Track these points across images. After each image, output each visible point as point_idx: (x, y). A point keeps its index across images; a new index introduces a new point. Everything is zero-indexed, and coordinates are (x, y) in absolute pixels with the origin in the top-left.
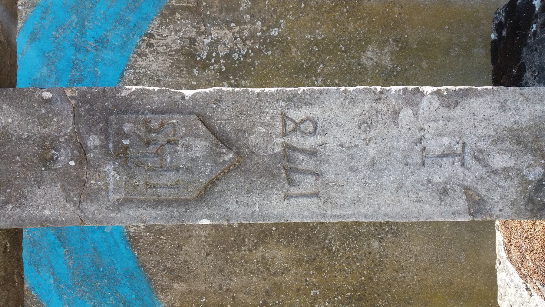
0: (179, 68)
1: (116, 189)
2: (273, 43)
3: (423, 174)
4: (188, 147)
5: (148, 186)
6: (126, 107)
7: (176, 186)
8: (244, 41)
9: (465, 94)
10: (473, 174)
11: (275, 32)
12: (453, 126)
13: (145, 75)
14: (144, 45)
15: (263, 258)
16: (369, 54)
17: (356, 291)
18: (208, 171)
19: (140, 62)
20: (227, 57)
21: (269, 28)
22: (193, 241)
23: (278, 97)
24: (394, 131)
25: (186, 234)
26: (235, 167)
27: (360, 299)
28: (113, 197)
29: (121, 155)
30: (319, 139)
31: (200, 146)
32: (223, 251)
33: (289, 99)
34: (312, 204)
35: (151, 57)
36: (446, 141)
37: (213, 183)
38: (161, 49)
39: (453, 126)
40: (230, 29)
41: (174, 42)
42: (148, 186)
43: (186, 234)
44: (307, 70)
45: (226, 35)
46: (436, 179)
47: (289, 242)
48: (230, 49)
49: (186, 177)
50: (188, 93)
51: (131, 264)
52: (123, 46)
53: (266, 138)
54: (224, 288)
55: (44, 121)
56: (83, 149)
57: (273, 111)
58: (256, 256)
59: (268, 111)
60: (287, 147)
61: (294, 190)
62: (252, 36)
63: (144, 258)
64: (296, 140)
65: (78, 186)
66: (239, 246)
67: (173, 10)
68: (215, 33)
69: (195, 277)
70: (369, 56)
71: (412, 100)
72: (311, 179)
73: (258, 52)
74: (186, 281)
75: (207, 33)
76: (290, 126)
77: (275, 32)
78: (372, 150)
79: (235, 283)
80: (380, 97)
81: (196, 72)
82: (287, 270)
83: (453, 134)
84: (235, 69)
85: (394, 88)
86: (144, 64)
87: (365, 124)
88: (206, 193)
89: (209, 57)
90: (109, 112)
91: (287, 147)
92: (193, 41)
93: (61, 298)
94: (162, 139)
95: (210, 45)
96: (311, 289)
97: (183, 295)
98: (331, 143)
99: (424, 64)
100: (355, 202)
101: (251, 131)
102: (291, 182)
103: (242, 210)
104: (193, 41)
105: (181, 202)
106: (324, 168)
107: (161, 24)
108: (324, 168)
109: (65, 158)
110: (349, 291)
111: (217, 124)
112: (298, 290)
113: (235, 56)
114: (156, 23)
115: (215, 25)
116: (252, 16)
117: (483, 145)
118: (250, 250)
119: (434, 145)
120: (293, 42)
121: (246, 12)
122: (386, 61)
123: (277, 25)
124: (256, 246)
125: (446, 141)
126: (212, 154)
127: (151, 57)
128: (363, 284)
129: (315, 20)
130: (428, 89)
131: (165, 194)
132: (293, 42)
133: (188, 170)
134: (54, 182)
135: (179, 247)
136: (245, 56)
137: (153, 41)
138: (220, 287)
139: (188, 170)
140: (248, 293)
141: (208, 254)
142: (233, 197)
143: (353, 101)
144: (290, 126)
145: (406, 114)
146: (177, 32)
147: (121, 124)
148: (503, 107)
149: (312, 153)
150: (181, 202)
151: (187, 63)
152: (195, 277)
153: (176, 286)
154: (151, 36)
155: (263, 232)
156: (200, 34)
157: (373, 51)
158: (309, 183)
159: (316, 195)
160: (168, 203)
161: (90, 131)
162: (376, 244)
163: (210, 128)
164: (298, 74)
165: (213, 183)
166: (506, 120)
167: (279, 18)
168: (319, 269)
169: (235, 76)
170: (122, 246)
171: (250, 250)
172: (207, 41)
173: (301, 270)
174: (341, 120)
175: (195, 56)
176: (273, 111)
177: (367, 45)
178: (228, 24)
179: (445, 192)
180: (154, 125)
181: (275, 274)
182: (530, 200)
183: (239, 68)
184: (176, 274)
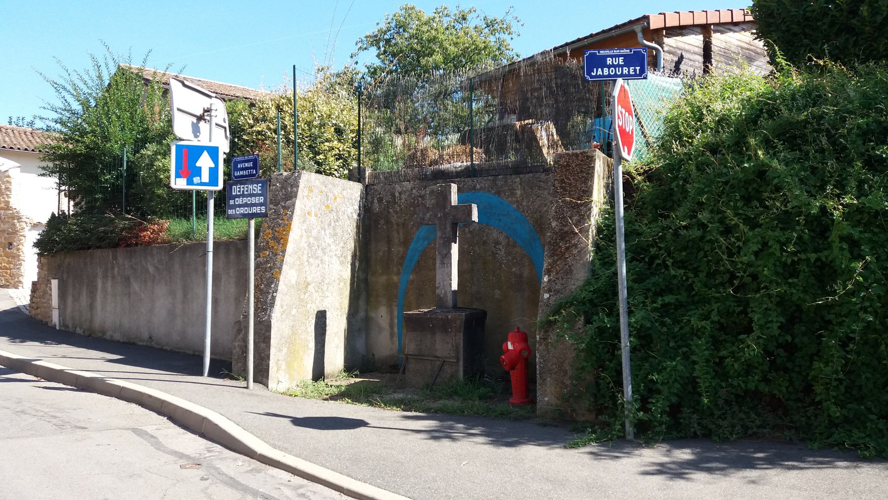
2: (500, 265)
65: (441, 237)
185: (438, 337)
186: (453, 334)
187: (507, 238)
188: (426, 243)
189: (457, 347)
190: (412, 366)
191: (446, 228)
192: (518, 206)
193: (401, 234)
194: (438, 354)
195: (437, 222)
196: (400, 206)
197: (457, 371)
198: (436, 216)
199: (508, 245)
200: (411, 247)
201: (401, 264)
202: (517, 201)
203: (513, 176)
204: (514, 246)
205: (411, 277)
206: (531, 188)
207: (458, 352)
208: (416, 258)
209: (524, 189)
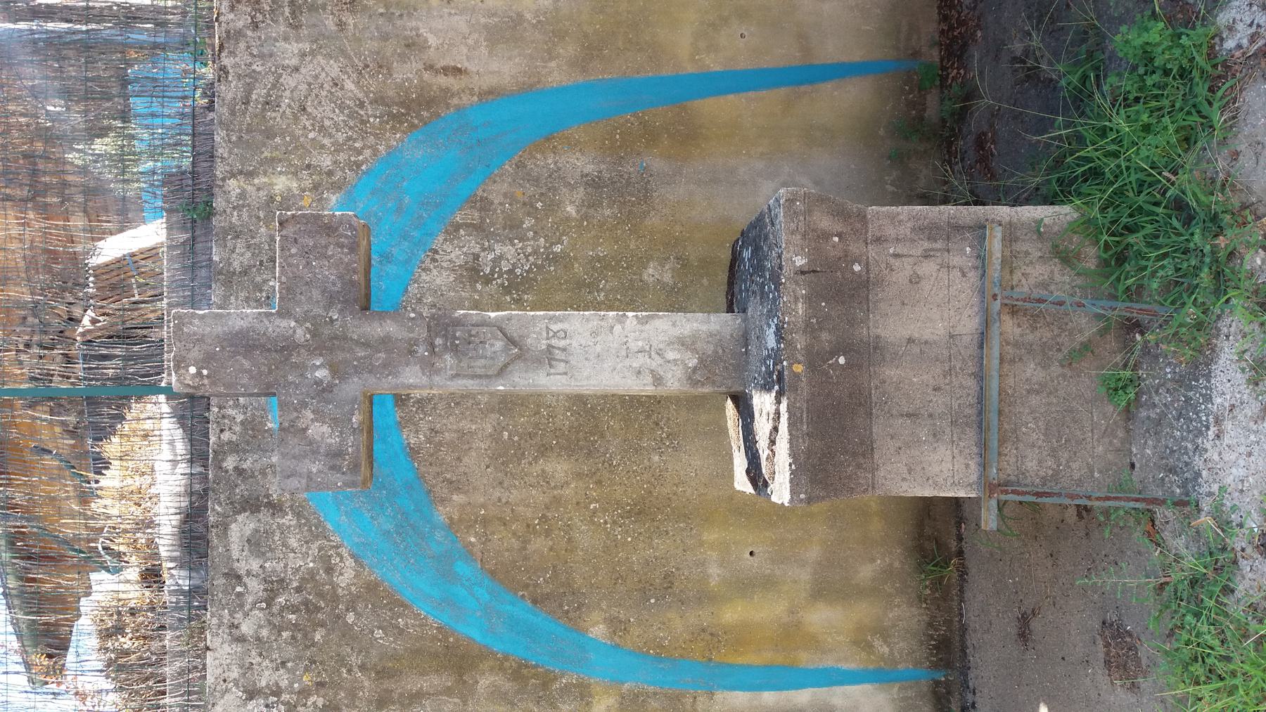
0: (462, 282)
1: (451, 368)
2: (555, 259)
3: (627, 362)
4: (492, 345)
5: (469, 367)
6: (458, 323)
7: (485, 367)
8: (527, 257)
9: (652, 317)
10: (656, 363)
11: (558, 248)
12: (644, 335)
13: (429, 289)
14: (428, 260)
15: (543, 471)
16: (651, 271)
17: (635, 505)
18: (502, 359)
19: (424, 276)
20: (511, 272)
21: (552, 244)
22: (474, 454)
23: (544, 317)
24: (611, 338)
25: (466, 447)
26: (519, 357)
27: (639, 513)
28: (450, 373)
29: (455, 350)
30: (568, 341)
31: (499, 345)
32: (503, 464)
33: (551, 319)
34: (563, 379)
35: (435, 272)
36: (640, 343)
37: (506, 366)
38: (445, 265)
39: (644, 335)
40: (513, 245)
41: (458, 257)
42: (469, 367)
43: (466, 447)
44: (589, 286)
45: (509, 250)
46: (634, 365)
47: (569, 456)
48: (513, 265)
49: (491, 362)
50: (493, 315)
51: (411, 475)
52: (408, 261)
53: (537, 341)
54: (504, 500)
55: (411, 330)
56: (432, 345)
57: (542, 325)
58: (536, 469)
59: (538, 324)
60: (549, 346)
61: (552, 371)
62: (535, 252)
63: (423, 469)
64: (554, 342)
65: (429, 367)
66: (519, 460)
67: (457, 227)
68: (499, 249)
69: (474, 488)
70: (651, 273)
71: (621, 320)
72: (563, 364)
73: (540, 267)
74: (465, 493)
75: (491, 249)
76: (551, 334)
77: (558, 248)
78: (598, 348)
79: (515, 495)
80: (603, 318)
81: (479, 287)
82: (567, 483)
83: (644, 339)
84: (518, 284)
85: (611, 313)
86: (428, 278)
87: (594, 333)
88: (502, 372)
89: (492, 272)
90: (448, 325)
91: (549, 346)
92: (476, 257)
93: (339, 509)
94: (477, 340)
95: (493, 261)
96: (590, 503)
97: (462, 507)
98: (575, 344)
99: (705, 281)
100: (588, 378)
101: (528, 337)
102: (551, 366)
103: (522, 382)
104: (476, 257)
105: (488, 377)
106: (570, 358)
107: (445, 240)
108: (570, 358)
109: (422, 351)
110: (628, 504)
111: (508, 332)
112: (578, 503)
113: (518, 271)
114: (441, 239)
115: (498, 241)
116: (535, 233)
117: (661, 346)
118: (531, 464)
119: (634, 346)
120: (576, 259)
121: (529, 229)
122: (668, 278)
123: (560, 242)
124: (536, 459)
125: (640, 343)
126: (506, 349)
127: (435, 272)
128: (643, 498)
129: (598, 238)
130: (630, 314)
131: (479, 371)
132: (576, 259)
133: (492, 358)
134: (415, 364)
135: (459, 459)
136: (527, 272)
137: (437, 257)
138: (500, 500)
139: (492, 358)
140: (528, 506)
141: (488, 467)
142: (517, 374)
143: (588, 320)
144: (551, 334)
145: (618, 328)
146: (460, 248)
147: (454, 332)
148: (674, 325)
149: (564, 350)
150: (488, 377)
151: (471, 278)
152: (474, 488)
153: (455, 497)
154: (436, 252)
155: (543, 445)
156: (484, 250)
157: (655, 268)
158: (561, 367)
159: (566, 374)
160: (480, 377)
161: (436, 336)
162: (656, 458)
163: (505, 335)
164: (580, 289)
165: (506, 366)
166: (676, 332)
167: (562, 235)
168: (599, 482)
169: (517, 291)
170: (402, 457)
171: (531, 464)
172: (490, 257)
173: (581, 484)
174: (581, 331)
175: (479, 271)
176: (542, 325)
177: (648, 262)
178: (511, 240)
179: (639, 372)
180: (473, 333)
181: (555, 487)
182: (690, 378)
183: (522, 283)
184: (454, 486)
185: (892, 326)
186: (872, 251)
187: (453, 230)
188: (462, 568)
189: (930, 231)
190: (1031, 465)
191: (386, 341)
192: (336, 187)
193: (424, 684)
194: (969, 325)
195: (353, 387)
196: (304, 693)
197: (1037, 229)
198: (323, 391)
199: (478, 229)
200: (476, 635)
201: (547, 679)
202: (316, 187)
203: (219, 203)
204: (484, 205)
205: (598, 631)
206: (269, 134)
207: (957, 228)
208: (522, 610)
209: (272, 161)
